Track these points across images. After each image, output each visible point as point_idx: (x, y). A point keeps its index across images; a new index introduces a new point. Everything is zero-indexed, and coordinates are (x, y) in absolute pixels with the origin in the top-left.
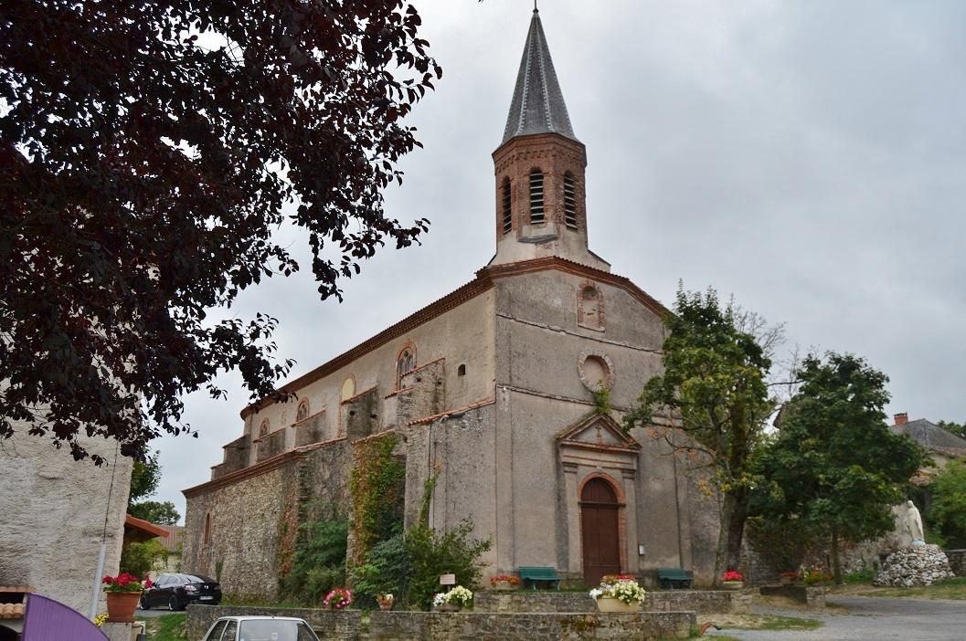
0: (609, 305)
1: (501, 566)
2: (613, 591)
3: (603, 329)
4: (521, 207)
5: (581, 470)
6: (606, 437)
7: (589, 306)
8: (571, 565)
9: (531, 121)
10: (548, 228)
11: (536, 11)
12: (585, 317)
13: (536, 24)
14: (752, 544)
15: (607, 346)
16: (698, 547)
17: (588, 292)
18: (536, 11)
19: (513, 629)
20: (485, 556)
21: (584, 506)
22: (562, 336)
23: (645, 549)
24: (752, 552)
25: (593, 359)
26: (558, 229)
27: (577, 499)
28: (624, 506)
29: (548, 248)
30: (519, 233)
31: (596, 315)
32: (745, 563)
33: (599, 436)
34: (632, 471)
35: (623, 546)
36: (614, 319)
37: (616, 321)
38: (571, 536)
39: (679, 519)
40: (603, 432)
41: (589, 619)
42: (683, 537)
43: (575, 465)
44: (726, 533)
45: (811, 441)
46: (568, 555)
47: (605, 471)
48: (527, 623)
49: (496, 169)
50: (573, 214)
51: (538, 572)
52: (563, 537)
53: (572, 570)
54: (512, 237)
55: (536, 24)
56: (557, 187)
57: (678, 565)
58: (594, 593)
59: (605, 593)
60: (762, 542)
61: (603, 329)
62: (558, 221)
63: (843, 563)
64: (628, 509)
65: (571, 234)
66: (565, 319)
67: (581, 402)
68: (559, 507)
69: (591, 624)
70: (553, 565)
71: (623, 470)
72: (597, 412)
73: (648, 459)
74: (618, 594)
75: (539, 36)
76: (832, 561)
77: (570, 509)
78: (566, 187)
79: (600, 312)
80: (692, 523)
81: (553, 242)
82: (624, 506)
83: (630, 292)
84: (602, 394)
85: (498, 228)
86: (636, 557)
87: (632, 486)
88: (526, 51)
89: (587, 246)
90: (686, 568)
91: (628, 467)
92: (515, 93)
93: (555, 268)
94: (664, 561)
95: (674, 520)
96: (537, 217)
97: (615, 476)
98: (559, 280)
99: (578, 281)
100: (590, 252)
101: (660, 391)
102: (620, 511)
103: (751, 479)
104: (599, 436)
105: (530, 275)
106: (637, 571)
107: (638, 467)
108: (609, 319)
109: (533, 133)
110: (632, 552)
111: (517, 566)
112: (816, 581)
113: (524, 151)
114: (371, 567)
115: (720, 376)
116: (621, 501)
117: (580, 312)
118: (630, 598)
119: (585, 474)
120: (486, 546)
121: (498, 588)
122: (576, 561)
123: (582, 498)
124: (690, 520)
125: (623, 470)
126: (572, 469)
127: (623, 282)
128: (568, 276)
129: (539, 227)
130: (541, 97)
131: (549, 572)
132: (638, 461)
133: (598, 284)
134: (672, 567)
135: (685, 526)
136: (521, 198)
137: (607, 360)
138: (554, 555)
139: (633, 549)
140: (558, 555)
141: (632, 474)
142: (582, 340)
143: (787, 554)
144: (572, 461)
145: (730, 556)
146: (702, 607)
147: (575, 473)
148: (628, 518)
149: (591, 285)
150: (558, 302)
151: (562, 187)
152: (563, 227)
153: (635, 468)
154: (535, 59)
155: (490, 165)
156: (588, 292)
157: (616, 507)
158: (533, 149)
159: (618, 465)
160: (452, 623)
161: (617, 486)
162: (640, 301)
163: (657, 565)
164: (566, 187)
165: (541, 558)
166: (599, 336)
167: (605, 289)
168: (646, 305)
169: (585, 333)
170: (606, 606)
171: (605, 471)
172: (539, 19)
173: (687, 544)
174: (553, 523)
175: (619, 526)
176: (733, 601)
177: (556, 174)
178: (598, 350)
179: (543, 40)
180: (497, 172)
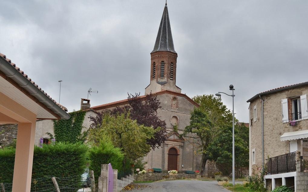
0: (180, 102)
1: (149, 167)
2: (172, 172)
3: (177, 109)
4: (158, 72)
5: (169, 145)
6: (176, 137)
7: (174, 102)
8: (165, 168)
9: (162, 46)
10: (165, 80)
11: (166, 4)
12: (173, 105)
13: (166, 8)
14: (217, 166)
15: (178, 113)
16: (198, 166)
17: (175, 99)
18: (166, 4)
19: (154, 178)
20: (146, 165)
21: (169, 154)
22: (166, 112)
23: (184, 166)
24: (217, 169)
25: (175, 117)
26: (168, 80)
27: (167, 153)
28: (179, 155)
29: (165, 86)
30: (157, 80)
31: (176, 105)
32: (215, 172)
33: (174, 137)
34: (182, 146)
35: (178, 164)
36: (180, 106)
37: (181, 106)
38: (165, 162)
39: (193, 159)
40: (175, 136)
41: (168, 176)
42: (194, 163)
43: (168, 144)
44: (202, 163)
45: (219, 144)
46: (164, 166)
47: (175, 146)
48: (157, 177)
49: (151, 58)
50: (172, 75)
51: (157, 169)
52: (163, 161)
53: (165, 169)
54: (154, 81)
55: (166, 8)
56: (168, 68)
57: (192, 170)
58: (169, 172)
59: (171, 172)
60: (220, 166)
61: (177, 109)
62: (168, 78)
63: (244, 173)
64: (180, 156)
65: (171, 81)
66: (168, 107)
67: (170, 128)
68: (163, 154)
69: (168, 177)
70: (161, 168)
71: (180, 146)
72: (174, 131)
73: (186, 143)
74: (173, 172)
75: (166, 14)
76: (241, 173)
77: (165, 155)
78: (171, 67)
79: (177, 104)
80: (197, 160)
81: (166, 84)
82: (179, 155)
83: (186, 98)
84: (176, 126)
85: (151, 77)
86: (181, 168)
87: (182, 150)
88: (163, 15)
89: (175, 84)
90: (194, 171)
91: (181, 145)
92: (159, 31)
93: (166, 93)
94: (188, 169)
95: (192, 158)
96: (162, 76)
97: (177, 147)
98: (167, 96)
99: (172, 96)
100: (176, 86)
101: (189, 130)
102: (178, 156)
103: (205, 152)
104: (174, 137)
105: (160, 95)
106: (181, 171)
107: (184, 145)
108: (179, 106)
109: (163, 50)
110: (180, 166)
111: (152, 168)
112: (217, 174)
113: (160, 56)
114: (121, 166)
115: (200, 130)
116: (178, 153)
117: (172, 105)
118: (174, 173)
119: (170, 146)
120: (146, 163)
121: (149, 172)
122: (166, 167)
123: (169, 153)
124: (196, 159)
125: (180, 146)
126: (167, 145)
127: (184, 96)
128: (169, 95)
129: (162, 79)
130: (166, 37)
131: (160, 169)
132: (184, 144)
133: (177, 96)
134: (190, 170)
135: (195, 160)
136: (158, 70)
137: (178, 117)
138: (161, 166)
139: (180, 165)
140: (162, 166)
141: (182, 147)
142: (172, 112)
143: (227, 170)
144: (167, 143)
145: (202, 168)
146: (190, 177)
147: (167, 146)
148: (180, 158)
149: (175, 97)
150: (166, 102)
151: (170, 67)
152: (169, 79)
153: (183, 145)
154: (165, 27)
155: (150, 57)
156: (175, 99)
157: (177, 155)
158: (162, 55)
159: (178, 145)
160: (142, 177)
161: (178, 150)
162: (189, 100)
163: (186, 170)
164: (171, 67)
165: (159, 167)
166: (176, 111)
167: (179, 98)
168: (190, 101)
169: (173, 110)
170: (171, 174)
171: (175, 146)
172: (167, 8)
173: (195, 165)
174: (161, 158)
175: (178, 158)
176: (197, 177)
177: (168, 63)
178: (175, 115)
179: (168, 16)
180: (152, 59)
